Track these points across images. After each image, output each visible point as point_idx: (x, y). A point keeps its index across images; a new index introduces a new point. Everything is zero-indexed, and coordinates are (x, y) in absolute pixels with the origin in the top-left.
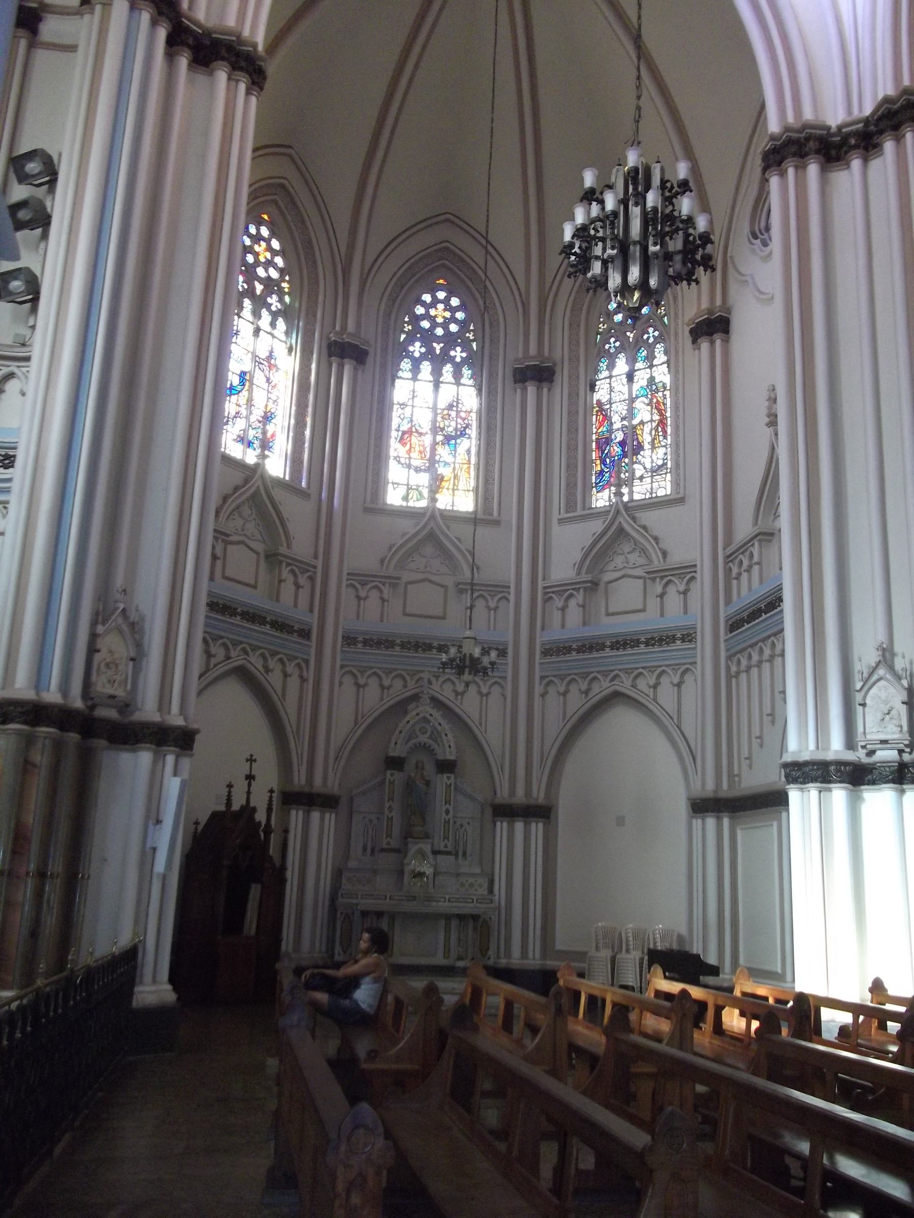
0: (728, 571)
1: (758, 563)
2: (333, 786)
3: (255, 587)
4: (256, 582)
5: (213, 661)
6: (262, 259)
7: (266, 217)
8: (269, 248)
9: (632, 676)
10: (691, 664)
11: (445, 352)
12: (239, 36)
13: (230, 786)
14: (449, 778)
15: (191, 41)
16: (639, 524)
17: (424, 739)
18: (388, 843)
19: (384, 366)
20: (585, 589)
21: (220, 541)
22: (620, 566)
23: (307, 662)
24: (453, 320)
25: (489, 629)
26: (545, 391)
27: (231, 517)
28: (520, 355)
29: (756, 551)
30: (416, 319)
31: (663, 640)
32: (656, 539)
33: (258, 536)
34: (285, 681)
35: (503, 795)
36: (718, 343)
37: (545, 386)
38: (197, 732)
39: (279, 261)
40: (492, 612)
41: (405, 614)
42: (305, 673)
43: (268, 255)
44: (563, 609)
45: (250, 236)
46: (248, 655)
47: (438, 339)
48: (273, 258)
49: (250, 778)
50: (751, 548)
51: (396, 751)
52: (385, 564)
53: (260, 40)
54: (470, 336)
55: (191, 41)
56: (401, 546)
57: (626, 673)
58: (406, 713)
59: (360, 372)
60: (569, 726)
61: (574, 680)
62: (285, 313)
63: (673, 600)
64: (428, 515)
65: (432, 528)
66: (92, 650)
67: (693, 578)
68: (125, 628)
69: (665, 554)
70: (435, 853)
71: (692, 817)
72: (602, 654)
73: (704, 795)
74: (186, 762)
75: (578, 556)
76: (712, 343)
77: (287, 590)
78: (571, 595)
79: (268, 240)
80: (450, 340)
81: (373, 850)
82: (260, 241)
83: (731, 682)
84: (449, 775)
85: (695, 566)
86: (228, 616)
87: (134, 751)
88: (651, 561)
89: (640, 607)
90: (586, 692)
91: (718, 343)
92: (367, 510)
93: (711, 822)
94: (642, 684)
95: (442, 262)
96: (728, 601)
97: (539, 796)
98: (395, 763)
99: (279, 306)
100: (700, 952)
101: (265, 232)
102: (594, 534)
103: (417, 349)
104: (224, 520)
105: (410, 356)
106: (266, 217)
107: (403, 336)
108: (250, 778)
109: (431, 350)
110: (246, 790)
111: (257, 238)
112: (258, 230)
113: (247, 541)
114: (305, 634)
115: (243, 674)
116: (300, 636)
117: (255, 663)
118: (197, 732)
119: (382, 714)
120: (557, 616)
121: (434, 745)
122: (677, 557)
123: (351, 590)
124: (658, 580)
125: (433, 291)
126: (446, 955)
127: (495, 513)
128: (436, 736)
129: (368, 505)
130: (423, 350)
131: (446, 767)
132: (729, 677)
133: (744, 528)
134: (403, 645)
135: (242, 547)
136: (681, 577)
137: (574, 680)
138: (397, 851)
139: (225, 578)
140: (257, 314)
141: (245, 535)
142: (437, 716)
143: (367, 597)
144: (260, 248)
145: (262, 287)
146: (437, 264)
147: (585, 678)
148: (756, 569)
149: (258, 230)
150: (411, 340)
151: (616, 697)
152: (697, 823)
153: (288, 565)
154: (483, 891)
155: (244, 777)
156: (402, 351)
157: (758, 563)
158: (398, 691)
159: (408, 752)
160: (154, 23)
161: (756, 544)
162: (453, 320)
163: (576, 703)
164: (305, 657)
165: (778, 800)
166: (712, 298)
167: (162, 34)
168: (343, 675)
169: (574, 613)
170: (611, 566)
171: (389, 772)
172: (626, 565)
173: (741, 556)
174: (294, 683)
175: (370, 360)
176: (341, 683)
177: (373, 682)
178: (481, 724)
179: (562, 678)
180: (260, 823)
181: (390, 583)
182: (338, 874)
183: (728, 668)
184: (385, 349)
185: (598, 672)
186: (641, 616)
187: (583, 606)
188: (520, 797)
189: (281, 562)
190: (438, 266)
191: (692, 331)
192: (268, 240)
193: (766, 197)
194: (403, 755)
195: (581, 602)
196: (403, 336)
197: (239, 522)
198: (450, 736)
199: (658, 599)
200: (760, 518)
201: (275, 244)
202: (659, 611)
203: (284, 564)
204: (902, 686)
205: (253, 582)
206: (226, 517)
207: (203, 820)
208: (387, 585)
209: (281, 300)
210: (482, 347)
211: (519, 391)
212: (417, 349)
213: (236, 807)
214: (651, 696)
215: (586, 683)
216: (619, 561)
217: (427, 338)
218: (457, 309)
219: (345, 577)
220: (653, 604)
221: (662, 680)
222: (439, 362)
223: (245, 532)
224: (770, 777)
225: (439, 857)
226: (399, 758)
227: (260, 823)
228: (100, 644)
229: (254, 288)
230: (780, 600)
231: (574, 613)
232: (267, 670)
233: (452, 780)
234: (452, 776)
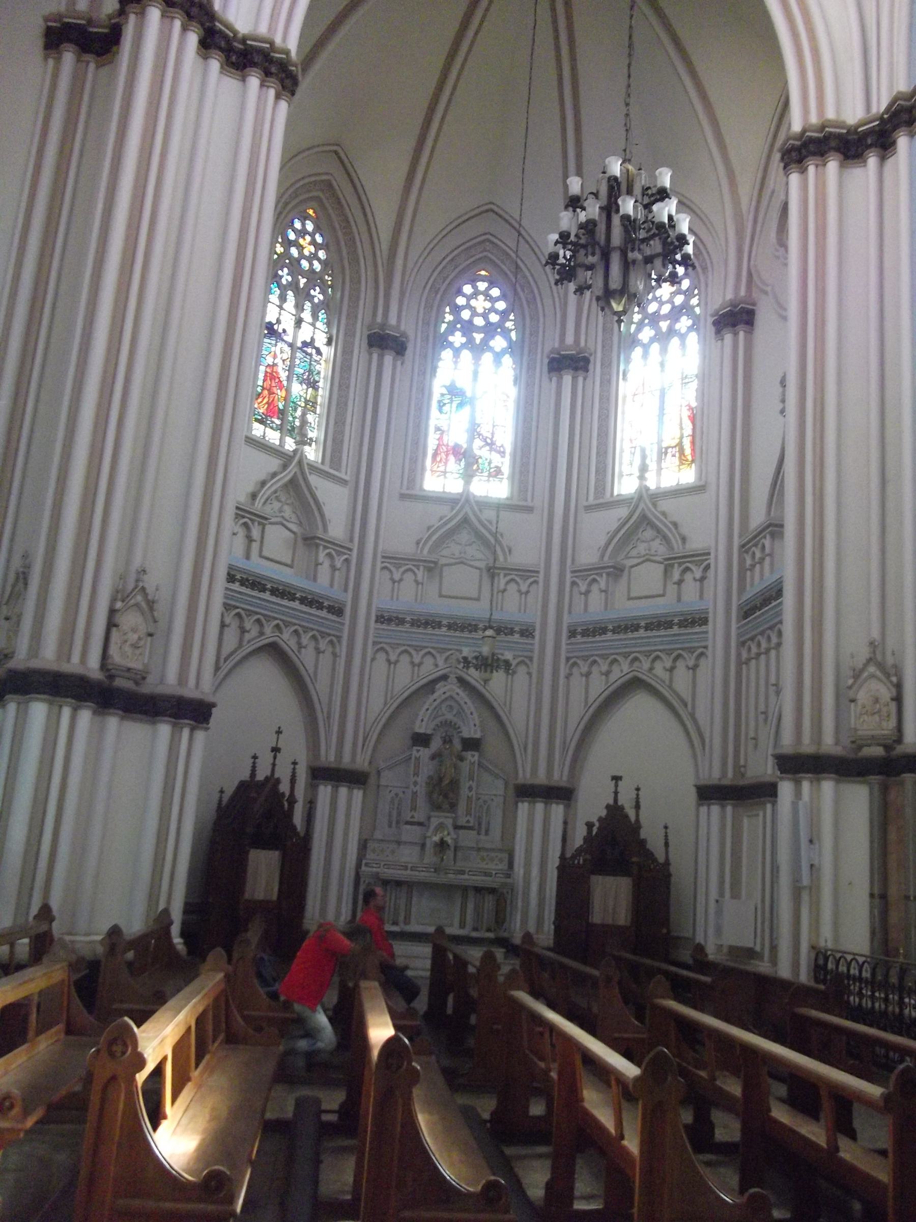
0: (742, 561)
1: (769, 555)
2: (362, 762)
5: (247, 637)
6: (306, 253)
7: (311, 212)
8: (313, 242)
9: (695, 654)
11: (485, 342)
12: (272, 43)
13: (255, 757)
14: (473, 756)
15: (223, 44)
16: (659, 510)
17: (449, 716)
18: (412, 817)
19: (425, 356)
20: (608, 574)
21: (256, 524)
22: (643, 553)
23: (339, 638)
24: (493, 310)
26: (581, 379)
27: (269, 501)
28: (557, 345)
29: (767, 542)
30: (456, 310)
32: (675, 525)
33: (294, 519)
34: (317, 660)
35: (525, 776)
36: (741, 335)
37: (580, 372)
38: (213, 705)
39: (322, 254)
40: (523, 596)
41: (441, 596)
42: (338, 650)
43: (312, 249)
44: (587, 593)
45: (294, 230)
46: (281, 633)
47: (479, 330)
48: (316, 251)
49: (276, 750)
50: (763, 540)
51: (420, 728)
52: (421, 545)
53: (292, 45)
54: (509, 325)
55: (223, 44)
56: (439, 528)
58: (433, 692)
59: (399, 363)
60: (591, 710)
62: (325, 305)
63: (690, 589)
64: (463, 500)
65: (466, 513)
66: (111, 624)
68: (144, 604)
69: (684, 539)
70: (457, 827)
71: (699, 805)
73: (710, 783)
74: (200, 735)
75: (602, 541)
76: (736, 334)
77: (324, 571)
79: (312, 235)
80: (490, 330)
81: (398, 822)
82: (305, 234)
83: (741, 669)
84: (473, 753)
85: (538, 572)
87: (154, 723)
88: (671, 548)
90: (607, 674)
91: (741, 335)
92: (403, 497)
93: (715, 809)
94: (659, 669)
95: (485, 253)
96: (742, 589)
97: (559, 777)
98: (421, 740)
99: (321, 297)
100: (702, 942)
101: (310, 226)
102: (619, 520)
103: (457, 339)
104: (260, 505)
105: (451, 345)
106: (311, 212)
107: (444, 327)
108: (276, 750)
109: (471, 341)
110: (272, 761)
111: (303, 233)
112: (303, 225)
113: (285, 522)
114: (337, 611)
115: (274, 651)
116: (329, 612)
117: (287, 639)
118: (213, 705)
119: (418, 690)
120: (579, 601)
121: (460, 723)
122: (696, 543)
123: (386, 572)
124: (676, 565)
125: (473, 282)
126: (462, 925)
127: (529, 499)
128: (460, 713)
129: (404, 491)
130: (464, 340)
131: (472, 744)
132: (740, 664)
133: (758, 517)
134: (450, 627)
135: (279, 527)
136: (698, 564)
138: (420, 824)
139: (261, 556)
140: (299, 307)
141: (283, 517)
142: (463, 696)
143: (401, 580)
144: (305, 241)
145: (305, 280)
146: (481, 255)
147: (648, 656)
148: (768, 559)
149: (303, 225)
150: (451, 329)
151: (634, 684)
152: (704, 810)
153: (325, 548)
154: (503, 866)
155: (270, 750)
156: (442, 342)
157: (769, 555)
158: (428, 670)
159: (434, 729)
160: (185, 29)
161: (768, 537)
162: (493, 310)
163: (598, 687)
164: (338, 634)
165: (769, 791)
166: (737, 287)
167: (193, 39)
168: (378, 650)
171: (415, 748)
173: (754, 548)
174: (325, 660)
175: (409, 352)
176: (373, 660)
177: (405, 659)
178: (505, 704)
180: (283, 794)
181: (425, 567)
182: (363, 846)
183: (739, 655)
184: (426, 339)
186: (660, 601)
188: (541, 778)
189: (317, 546)
190: (480, 259)
191: (715, 323)
192: (312, 235)
193: (281, 197)
194: (429, 732)
196: (444, 327)
197: (276, 505)
198: (475, 715)
200: (773, 510)
201: (319, 239)
202: (698, 594)
203: (321, 548)
204: (891, 682)
205: (289, 562)
206: (263, 501)
207: (230, 791)
208: (421, 568)
209: (323, 292)
210: (522, 339)
212: (457, 339)
213: (260, 777)
214: (667, 682)
215: (671, 660)
216: (642, 548)
217: (468, 328)
218: (497, 299)
219: (379, 559)
220: (672, 589)
222: (478, 350)
223: (283, 514)
224: (766, 770)
225: (461, 832)
226: (425, 734)
227: (283, 794)
228: (121, 619)
229: (298, 283)
230: (779, 593)
232: (300, 646)
233: (476, 758)
234: (476, 754)
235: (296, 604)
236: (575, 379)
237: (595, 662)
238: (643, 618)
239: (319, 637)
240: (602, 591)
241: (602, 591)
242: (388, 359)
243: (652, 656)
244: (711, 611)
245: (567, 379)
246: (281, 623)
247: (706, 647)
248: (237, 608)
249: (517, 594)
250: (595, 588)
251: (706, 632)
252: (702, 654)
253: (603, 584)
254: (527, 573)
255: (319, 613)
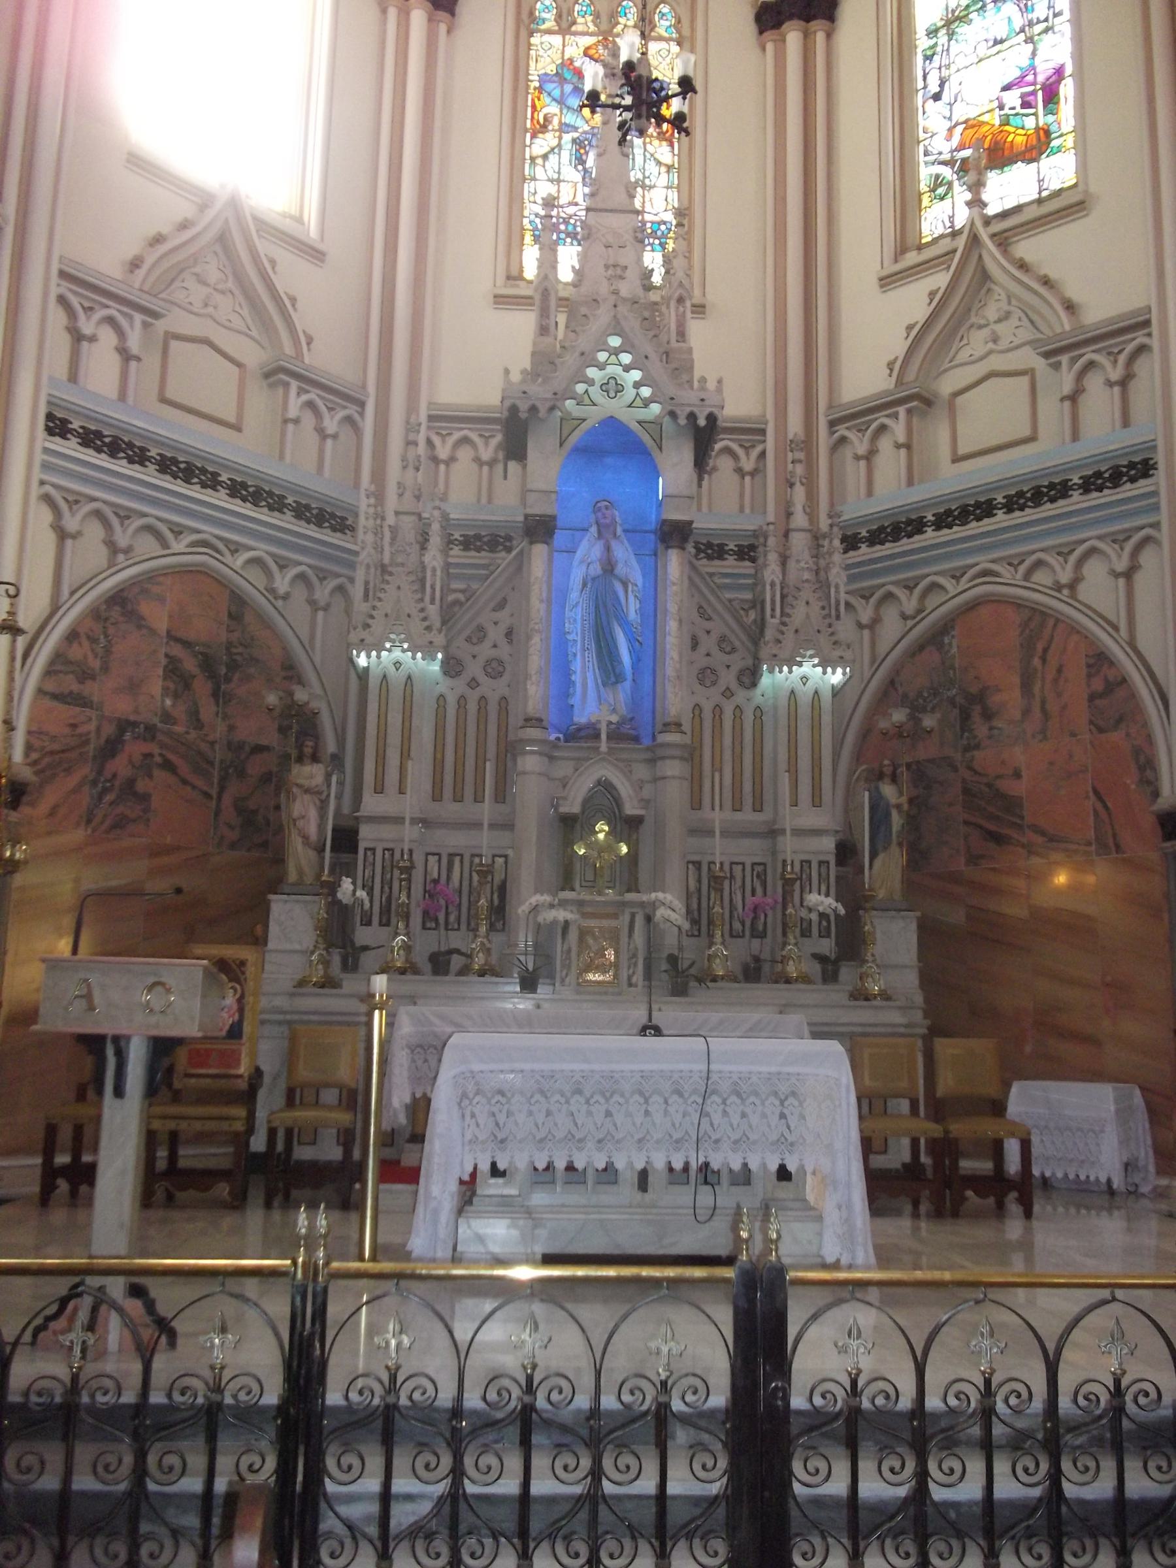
3: (238, 428)
4: (240, 416)
10: (1151, 526)
25: (742, 509)
26: (820, 37)
31: (1121, 475)
37: (818, 27)
44: (870, 456)
57: (1114, 541)
61: (1093, 551)
67: (1142, 349)
69: (1070, 307)
72: (918, 541)
75: (899, 347)
78: (883, 428)
86: (266, 510)
89: (1026, 432)
120: (854, 473)
137: (1093, 551)
169: (890, 463)
170: (963, 356)
172: (991, 345)
179: (1118, 540)
185: (1100, 538)
187: (908, 446)
195: (902, 439)
199: (1067, 404)
205: (232, 420)
211: (770, 47)
216: (977, 342)
221: (1086, 570)
223: (210, 310)
231: (890, 463)
235: (220, 498)
236: (806, 35)
237: (889, 596)
238: (997, 486)
239: (314, 580)
240: (898, 446)
241: (898, 446)
242: (694, 525)
243: (1027, 563)
244: (1160, 444)
245: (793, 36)
246: (309, 572)
247: (1156, 525)
248: (300, 564)
249: (736, 477)
250: (885, 444)
251: (1155, 494)
252: (1147, 540)
253: (899, 430)
254: (752, 432)
255: (207, 496)
